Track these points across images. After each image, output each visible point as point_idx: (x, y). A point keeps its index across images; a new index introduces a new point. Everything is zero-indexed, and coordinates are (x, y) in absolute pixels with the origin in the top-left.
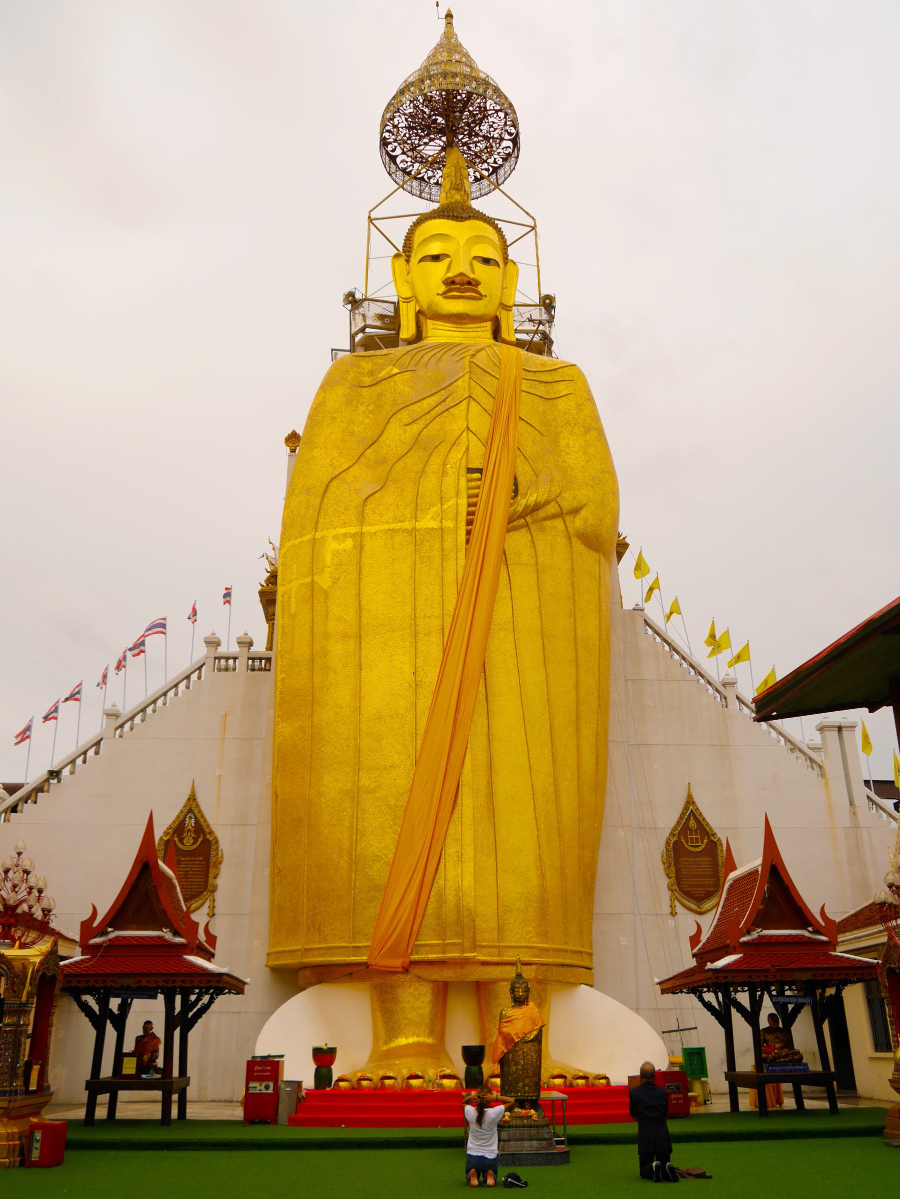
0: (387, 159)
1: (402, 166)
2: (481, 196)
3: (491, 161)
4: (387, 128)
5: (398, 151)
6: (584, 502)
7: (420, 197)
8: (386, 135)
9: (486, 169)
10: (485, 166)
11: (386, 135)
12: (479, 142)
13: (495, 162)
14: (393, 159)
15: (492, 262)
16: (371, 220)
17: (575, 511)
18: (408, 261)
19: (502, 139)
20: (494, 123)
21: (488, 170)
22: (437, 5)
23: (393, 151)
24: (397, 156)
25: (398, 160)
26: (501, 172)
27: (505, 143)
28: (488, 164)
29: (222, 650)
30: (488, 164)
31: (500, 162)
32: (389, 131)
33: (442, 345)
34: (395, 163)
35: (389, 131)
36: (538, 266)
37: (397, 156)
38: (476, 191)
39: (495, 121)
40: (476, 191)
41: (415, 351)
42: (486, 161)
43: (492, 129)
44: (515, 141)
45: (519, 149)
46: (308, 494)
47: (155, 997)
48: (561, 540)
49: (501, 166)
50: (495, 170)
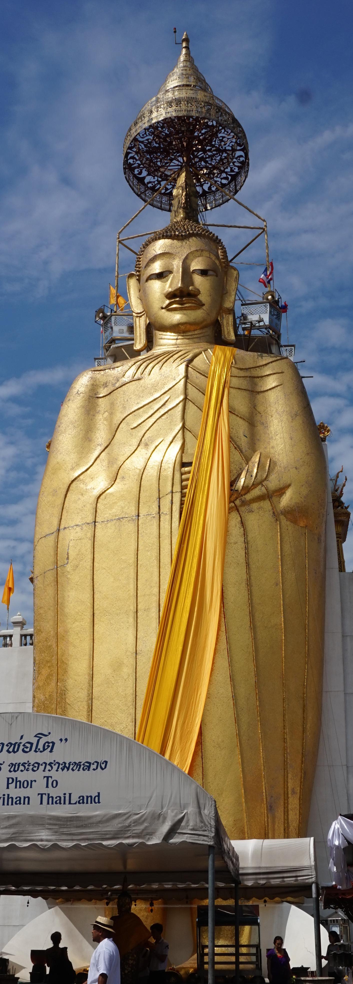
0: (135, 182)
1: (150, 185)
2: (223, 203)
3: (228, 170)
4: (130, 155)
5: (144, 173)
6: (289, 482)
8: (131, 161)
9: (224, 178)
10: (224, 175)
11: (131, 161)
12: (214, 155)
13: (232, 171)
14: (141, 180)
16: (120, 242)
17: (281, 491)
18: (139, 280)
20: (223, 137)
21: (226, 178)
23: (140, 173)
24: (144, 178)
25: (146, 181)
28: (226, 173)
30: (226, 173)
31: (236, 170)
32: (133, 158)
33: (164, 354)
34: (144, 184)
35: (133, 158)
37: (144, 178)
38: (220, 199)
39: (224, 135)
40: (220, 199)
41: (141, 362)
42: (223, 171)
43: (223, 143)
45: (248, 160)
46: (53, 495)
47: (293, 968)
48: (268, 517)
49: (238, 174)
50: (234, 178)
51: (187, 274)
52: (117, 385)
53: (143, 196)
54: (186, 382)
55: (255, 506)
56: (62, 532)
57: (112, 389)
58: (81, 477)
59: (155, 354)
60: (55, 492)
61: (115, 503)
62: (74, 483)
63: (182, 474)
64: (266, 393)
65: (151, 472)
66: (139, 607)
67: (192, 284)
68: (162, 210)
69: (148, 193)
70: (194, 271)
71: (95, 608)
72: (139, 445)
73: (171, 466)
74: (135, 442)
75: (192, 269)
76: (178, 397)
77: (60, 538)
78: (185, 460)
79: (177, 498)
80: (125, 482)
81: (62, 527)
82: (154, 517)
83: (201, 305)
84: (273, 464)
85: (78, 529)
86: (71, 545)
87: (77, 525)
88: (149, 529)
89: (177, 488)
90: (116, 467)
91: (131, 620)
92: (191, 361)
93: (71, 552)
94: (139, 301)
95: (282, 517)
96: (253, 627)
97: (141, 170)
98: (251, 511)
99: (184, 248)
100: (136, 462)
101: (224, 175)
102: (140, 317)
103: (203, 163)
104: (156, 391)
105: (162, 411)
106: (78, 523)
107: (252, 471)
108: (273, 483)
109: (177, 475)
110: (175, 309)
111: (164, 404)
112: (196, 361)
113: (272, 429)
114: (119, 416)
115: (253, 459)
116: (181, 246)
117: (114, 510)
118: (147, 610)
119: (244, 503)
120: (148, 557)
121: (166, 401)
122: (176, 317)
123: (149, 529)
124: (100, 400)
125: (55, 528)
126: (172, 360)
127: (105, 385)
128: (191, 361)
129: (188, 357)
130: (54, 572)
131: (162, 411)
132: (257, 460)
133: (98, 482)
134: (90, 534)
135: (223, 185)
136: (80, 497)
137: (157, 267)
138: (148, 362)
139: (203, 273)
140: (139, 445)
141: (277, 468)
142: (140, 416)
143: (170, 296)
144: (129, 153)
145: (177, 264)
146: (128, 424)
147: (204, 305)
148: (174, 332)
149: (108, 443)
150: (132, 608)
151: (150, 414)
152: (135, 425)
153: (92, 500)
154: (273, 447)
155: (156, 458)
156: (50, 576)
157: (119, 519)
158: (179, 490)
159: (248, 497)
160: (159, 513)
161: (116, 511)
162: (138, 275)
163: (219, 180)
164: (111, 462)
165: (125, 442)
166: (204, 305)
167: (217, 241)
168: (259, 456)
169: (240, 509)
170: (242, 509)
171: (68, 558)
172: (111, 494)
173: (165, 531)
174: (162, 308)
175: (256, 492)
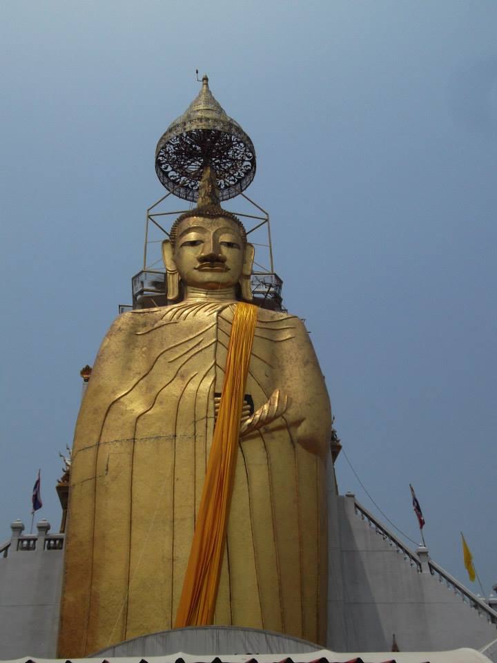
0: (161, 174)
1: (172, 178)
3: (236, 174)
4: (161, 154)
5: (169, 169)
7: (186, 199)
8: (160, 158)
11: (160, 158)
12: (227, 162)
13: (239, 175)
14: (166, 174)
15: (234, 245)
16: (149, 217)
17: (298, 423)
19: (243, 160)
20: (237, 150)
21: (234, 181)
22: (197, 72)
23: (166, 168)
24: (168, 172)
25: (170, 175)
26: (244, 182)
27: (245, 163)
29: (26, 534)
31: (243, 175)
32: (162, 156)
33: (197, 304)
34: (167, 177)
35: (162, 156)
36: (270, 246)
37: (168, 172)
44: (253, 162)
46: (94, 413)
49: (243, 178)
50: (240, 181)
51: (217, 245)
52: (156, 325)
53: (166, 185)
54: (217, 328)
55: (276, 434)
56: (101, 446)
57: (151, 328)
58: (122, 400)
59: (189, 304)
60: (96, 411)
61: (154, 423)
62: (115, 404)
63: (215, 403)
64: (282, 343)
65: (188, 399)
66: (175, 516)
67: (221, 252)
68: (180, 197)
69: (171, 184)
70: (222, 243)
71: (133, 516)
72: (175, 377)
73: (206, 395)
74: (172, 374)
75: (220, 241)
76: (211, 339)
77: (99, 452)
78: (217, 391)
79: (211, 422)
80: (164, 406)
81: (102, 441)
82: (190, 438)
83: (227, 270)
84: (290, 401)
85: (118, 444)
86: (110, 458)
87: (117, 441)
88: (185, 449)
89: (211, 414)
90: (154, 393)
91: (168, 529)
92: (220, 312)
93: (110, 465)
94: (173, 262)
95: (299, 447)
96: (276, 539)
97: (167, 166)
98: (273, 438)
99: (212, 226)
100: (174, 389)
101: (233, 178)
102: (173, 274)
103: (217, 167)
104: (191, 333)
105: (196, 350)
106: (117, 439)
107: (274, 405)
108: (292, 414)
109: (211, 403)
110: (206, 270)
111: (198, 344)
112: (224, 313)
113: (287, 372)
114: (157, 352)
115: (273, 395)
116: (211, 223)
117: (152, 430)
118: (183, 519)
119: (267, 431)
120: (184, 472)
121: (201, 342)
122: (208, 276)
123: (185, 449)
124: (140, 337)
125: (95, 442)
126: (204, 309)
127: (145, 325)
128: (220, 312)
129: (219, 308)
130: (93, 481)
131: (196, 350)
132: (277, 396)
133: (136, 406)
134: (129, 450)
135: (230, 186)
136: (120, 416)
137: (192, 236)
138: (183, 309)
139: (229, 245)
140: (175, 377)
141: (294, 404)
142: (177, 352)
143: (202, 260)
144: (160, 152)
145: (209, 237)
146: (165, 358)
147: (229, 269)
148: (204, 288)
149: (146, 372)
150: (170, 517)
151: (185, 351)
152: (172, 359)
153: (132, 420)
154: (289, 387)
155: (192, 387)
156: (88, 486)
157: (157, 438)
158: (213, 416)
159: (271, 426)
160: (195, 434)
161: (153, 430)
162: (173, 242)
163: (228, 181)
164: (150, 389)
165: (162, 374)
166: (229, 269)
167: (240, 224)
168: (278, 393)
169: (264, 436)
170: (265, 436)
171: (107, 470)
172: (150, 415)
173: (200, 451)
174: (195, 269)
175: (278, 422)
